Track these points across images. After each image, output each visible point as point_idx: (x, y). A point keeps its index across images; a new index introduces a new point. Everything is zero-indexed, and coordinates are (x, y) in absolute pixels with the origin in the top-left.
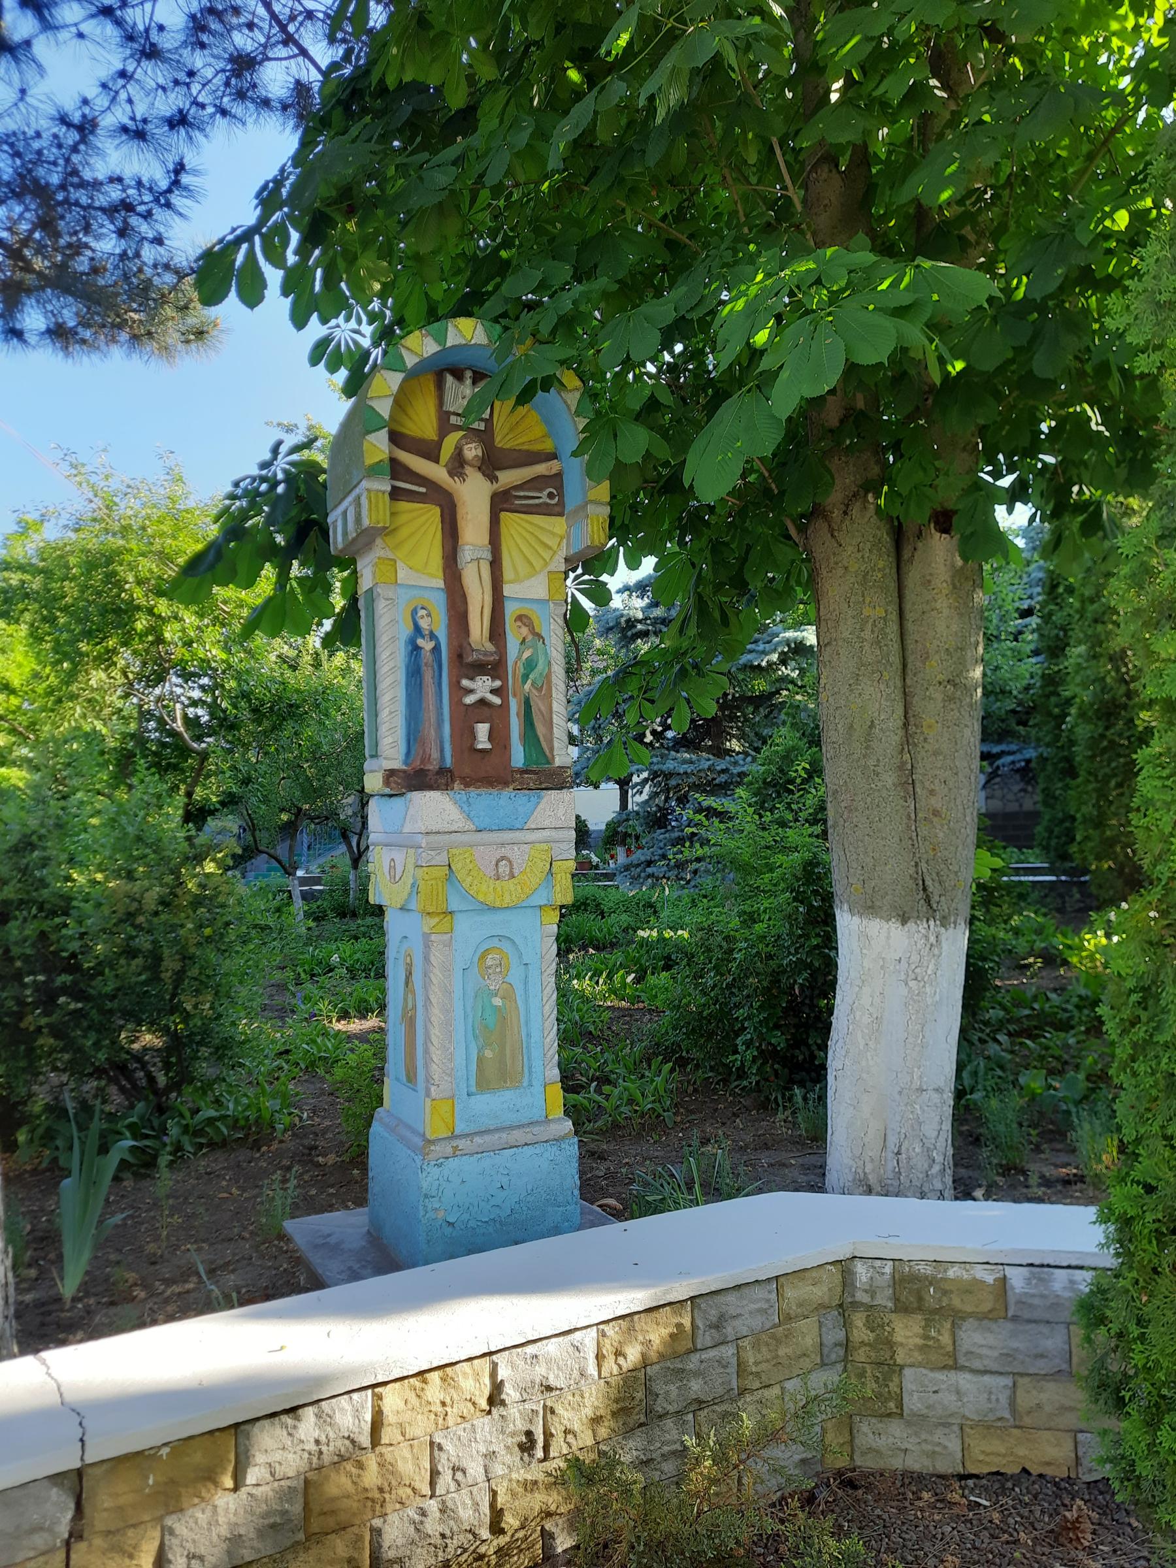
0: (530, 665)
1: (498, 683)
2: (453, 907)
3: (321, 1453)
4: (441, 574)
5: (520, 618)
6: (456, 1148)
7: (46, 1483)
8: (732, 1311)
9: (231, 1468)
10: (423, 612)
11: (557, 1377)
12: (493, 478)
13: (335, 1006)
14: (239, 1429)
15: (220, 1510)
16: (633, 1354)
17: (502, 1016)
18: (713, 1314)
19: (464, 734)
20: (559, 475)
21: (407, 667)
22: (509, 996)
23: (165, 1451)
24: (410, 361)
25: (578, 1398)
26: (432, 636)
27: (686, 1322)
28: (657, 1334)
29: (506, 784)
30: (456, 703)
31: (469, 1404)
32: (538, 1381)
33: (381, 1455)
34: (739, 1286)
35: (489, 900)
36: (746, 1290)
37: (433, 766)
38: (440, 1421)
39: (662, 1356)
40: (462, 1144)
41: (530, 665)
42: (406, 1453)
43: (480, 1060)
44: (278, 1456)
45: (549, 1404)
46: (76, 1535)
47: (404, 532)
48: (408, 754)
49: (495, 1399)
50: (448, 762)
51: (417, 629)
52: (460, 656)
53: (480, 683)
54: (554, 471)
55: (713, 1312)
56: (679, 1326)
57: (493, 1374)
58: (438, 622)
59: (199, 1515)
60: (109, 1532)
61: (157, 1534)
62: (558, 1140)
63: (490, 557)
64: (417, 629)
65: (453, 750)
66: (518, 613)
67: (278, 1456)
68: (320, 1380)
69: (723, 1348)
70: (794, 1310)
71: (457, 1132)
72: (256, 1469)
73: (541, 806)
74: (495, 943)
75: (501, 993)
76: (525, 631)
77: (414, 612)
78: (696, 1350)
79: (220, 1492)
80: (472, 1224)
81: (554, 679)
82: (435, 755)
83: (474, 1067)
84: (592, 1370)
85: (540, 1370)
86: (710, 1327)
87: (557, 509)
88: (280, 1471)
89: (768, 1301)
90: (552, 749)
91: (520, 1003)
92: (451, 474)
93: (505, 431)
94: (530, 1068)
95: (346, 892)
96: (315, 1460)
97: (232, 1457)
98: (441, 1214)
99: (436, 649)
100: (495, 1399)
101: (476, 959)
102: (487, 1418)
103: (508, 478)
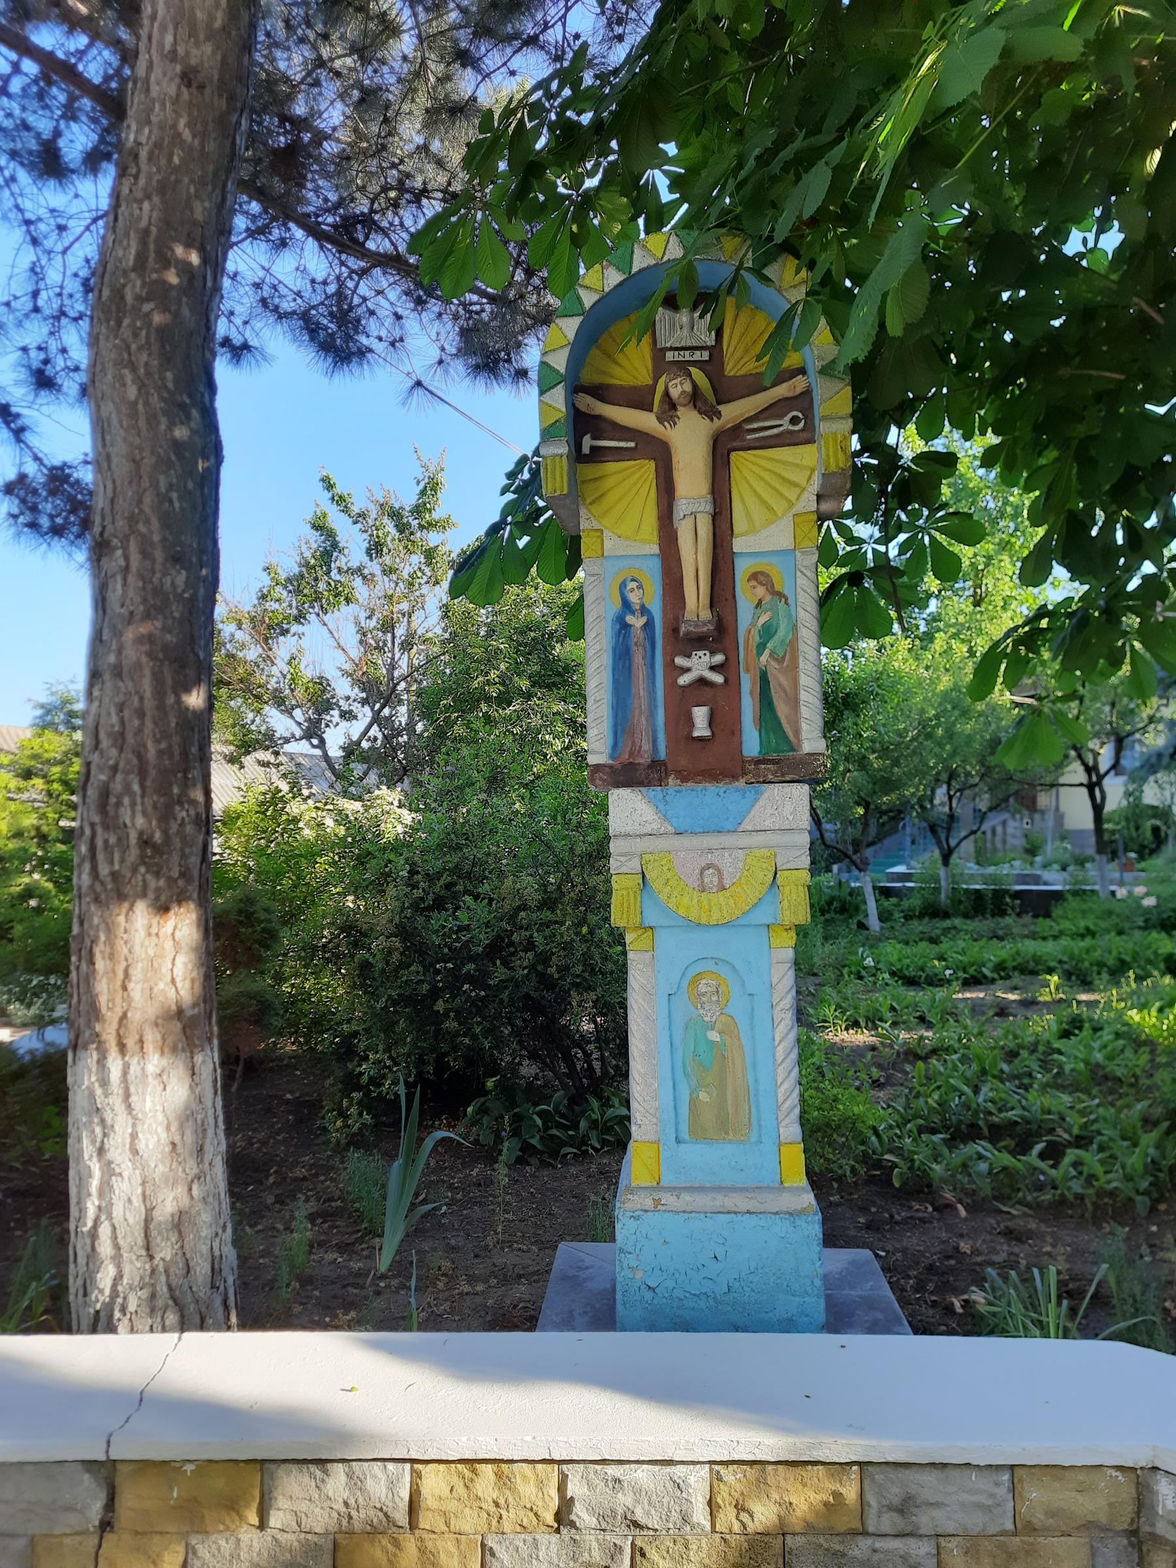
0: (768, 632)
1: (719, 658)
2: (650, 920)
3: (350, 1517)
4: (656, 538)
5: (754, 576)
6: (657, 1202)
7: (80, 1466)
8: (928, 1495)
9: (255, 1505)
10: (634, 585)
11: (648, 1514)
12: (711, 413)
13: (843, 1013)
14: (264, 1467)
15: (242, 1545)
16: (764, 1514)
17: (721, 1055)
18: (895, 1494)
19: (680, 719)
20: (807, 393)
21: (614, 649)
22: (729, 1029)
23: (189, 1468)
24: (589, 299)
25: (680, 1547)
26: (644, 610)
27: (850, 1492)
28: (804, 1499)
29: (735, 777)
30: (671, 684)
31: (531, 1515)
32: (620, 1511)
33: (422, 1540)
34: (945, 1465)
35: (693, 915)
36: (953, 1473)
37: (644, 759)
38: (494, 1523)
39: (810, 1529)
40: (668, 1199)
41: (768, 632)
42: (451, 1547)
43: (694, 1103)
44: (304, 1507)
45: (639, 1543)
46: (106, 1525)
47: (612, 497)
48: (615, 746)
49: (563, 1517)
50: (662, 754)
51: (626, 604)
52: (676, 630)
53: (695, 658)
54: (799, 390)
55: (896, 1490)
56: (837, 1495)
57: (562, 1488)
58: (652, 596)
59: (222, 1543)
60: (137, 1533)
61: (181, 1549)
62: (801, 1213)
63: (709, 508)
64: (626, 604)
65: (668, 739)
66: (753, 570)
67: (304, 1507)
68: (344, 1436)
69: (912, 1543)
70: (1039, 1518)
71: (664, 1183)
72: (281, 1513)
73: (761, 802)
74: (710, 965)
75: (718, 1026)
76: (761, 591)
77: (623, 585)
78: (865, 1533)
79: (245, 1527)
80: (678, 1293)
81: (802, 647)
82: (646, 746)
83: (684, 1110)
84: (700, 1515)
85: (624, 1500)
86: (890, 1508)
87: (805, 435)
88: (307, 1524)
89: (992, 1496)
90: (797, 732)
91: (745, 1041)
92: (661, 420)
93: (738, 354)
94: (759, 1120)
95: (937, 890)
96: (345, 1523)
97: (257, 1493)
98: (639, 1275)
99: (649, 626)
100: (563, 1517)
101: (685, 983)
102: (555, 1538)
103: (733, 412)
